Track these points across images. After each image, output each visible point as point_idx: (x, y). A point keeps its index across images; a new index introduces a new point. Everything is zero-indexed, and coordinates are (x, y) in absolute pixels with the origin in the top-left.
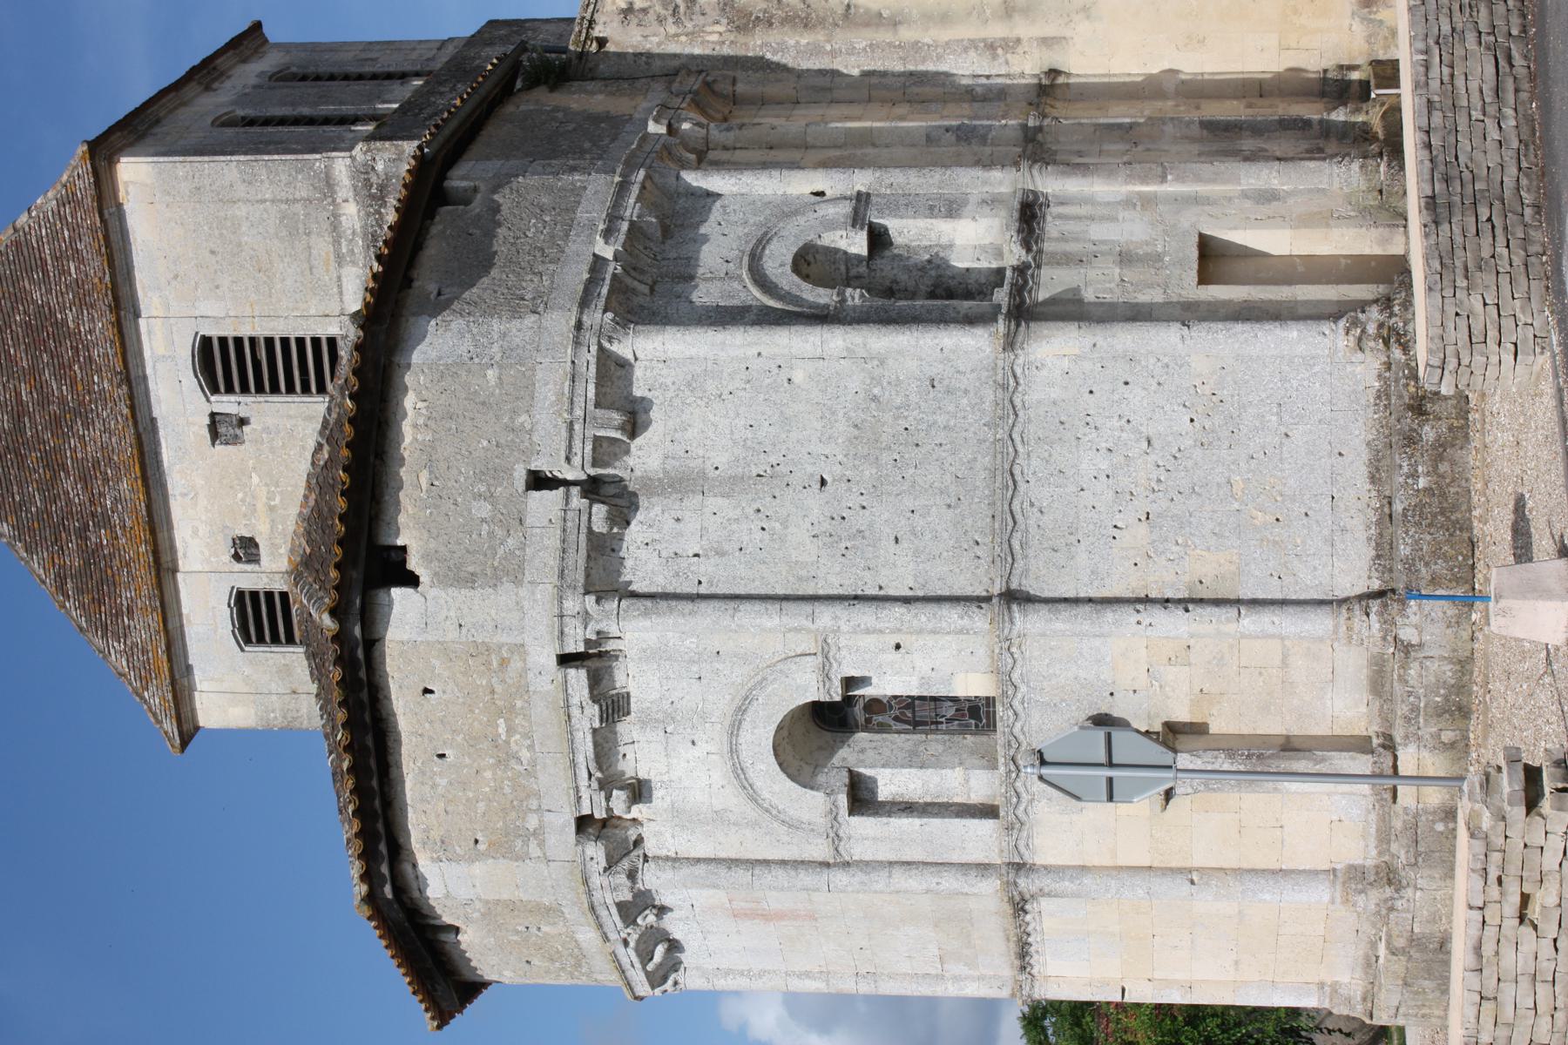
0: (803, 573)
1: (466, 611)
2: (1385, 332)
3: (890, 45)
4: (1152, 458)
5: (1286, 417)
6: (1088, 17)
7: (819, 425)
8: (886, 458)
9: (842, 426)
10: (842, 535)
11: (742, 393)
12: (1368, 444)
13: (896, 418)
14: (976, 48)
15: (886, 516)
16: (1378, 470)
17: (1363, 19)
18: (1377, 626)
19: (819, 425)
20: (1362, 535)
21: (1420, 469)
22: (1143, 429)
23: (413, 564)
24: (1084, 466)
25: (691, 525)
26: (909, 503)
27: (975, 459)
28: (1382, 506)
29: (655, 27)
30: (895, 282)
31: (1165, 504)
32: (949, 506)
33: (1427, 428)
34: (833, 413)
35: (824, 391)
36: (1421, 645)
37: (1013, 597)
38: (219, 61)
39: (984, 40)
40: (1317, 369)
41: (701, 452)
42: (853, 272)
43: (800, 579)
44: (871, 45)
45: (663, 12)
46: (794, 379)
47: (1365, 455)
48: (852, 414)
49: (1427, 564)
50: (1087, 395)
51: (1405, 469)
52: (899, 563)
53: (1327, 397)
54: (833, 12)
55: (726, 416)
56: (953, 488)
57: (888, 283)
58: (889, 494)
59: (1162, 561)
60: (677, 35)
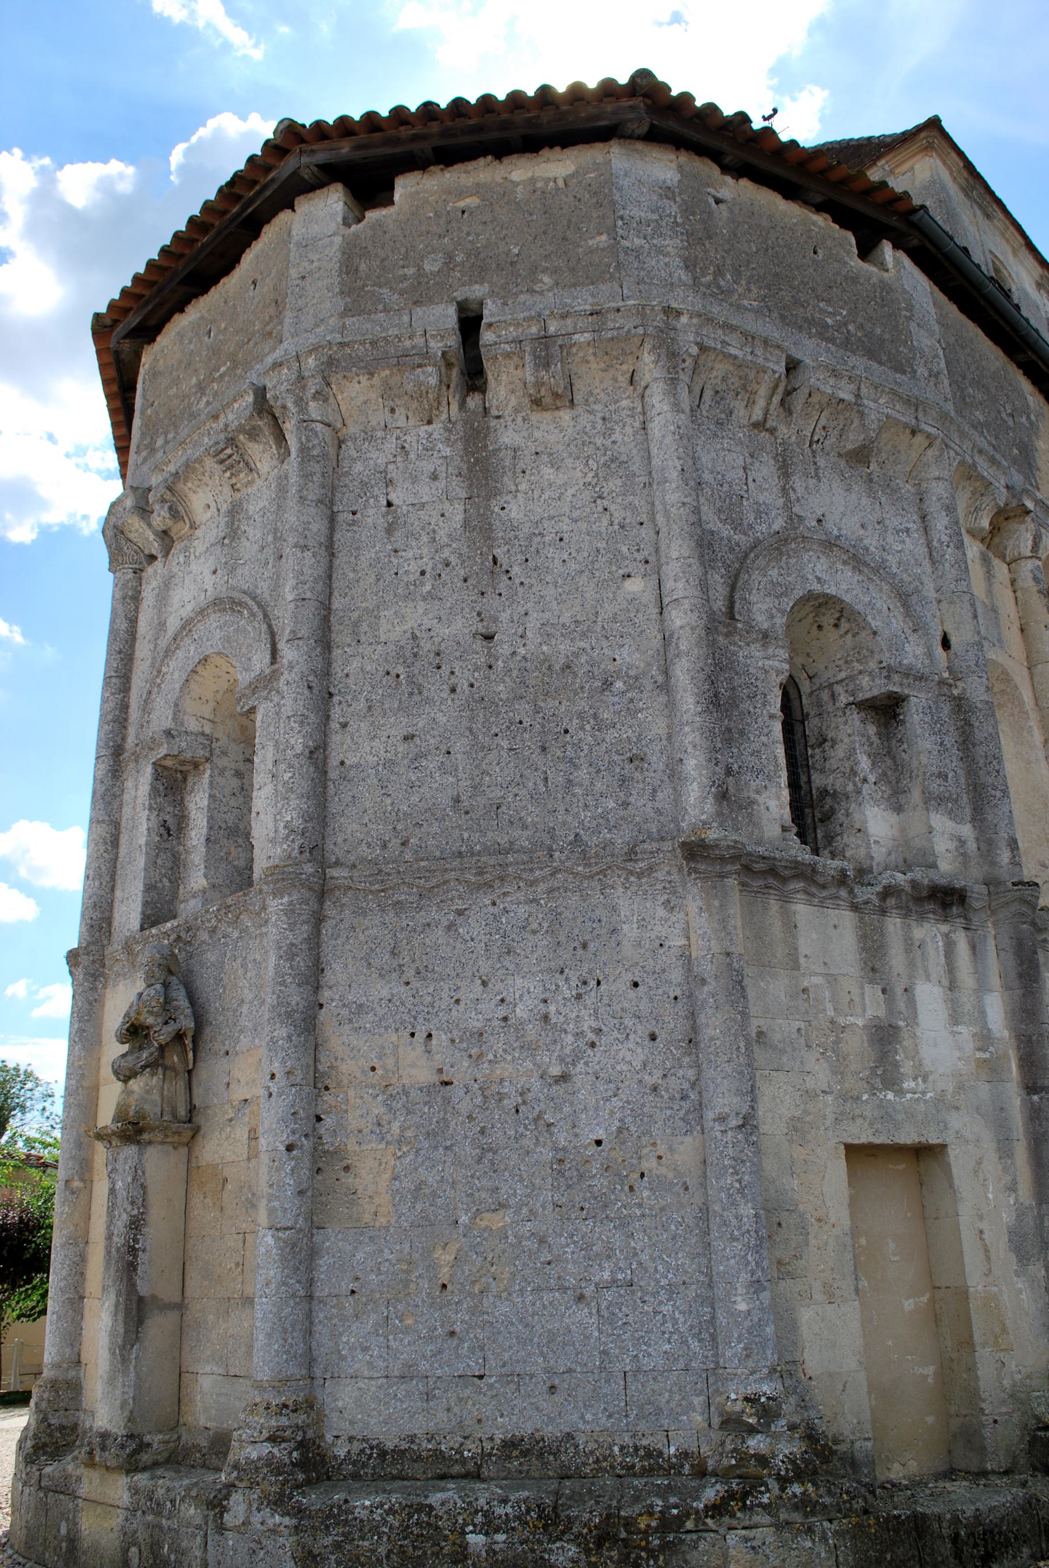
0: (364, 627)
1: (317, 275)
4: (536, 1084)
5: (608, 1296)
7: (566, 619)
8: (523, 710)
9: (565, 647)
10: (413, 669)
11: (605, 523)
12: (569, 1436)
13: (581, 716)
15: (442, 719)
16: (525, 1454)
18: (254, 1455)
19: (566, 619)
20: (419, 1426)
21: (501, 1537)
22: (580, 1066)
23: (372, 215)
24: (519, 982)
25: (426, 492)
26: (460, 746)
27: (525, 827)
28: (463, 1461)
30: (834, 743)
31: (464, 1107)
32: (457, 800)
33: (572, 1550)
34: (584, 635)
35: (614, 619)
36: (221, 1529)
37: (322, 892)
40: (694, 1345)
41: (523, 487)
42: (838, 689)
43: (356, 624)
47: (551, 1431)
48: (583, 659)
49: (337, 1546)
50: (629, 977)
51: (500, 1511)
52: (376, 743)
53: (647, 1363)
55: (574, 507)
56: (482, 801)
57: (831, 735)
58: (471, 719)
59: (378, 1109)
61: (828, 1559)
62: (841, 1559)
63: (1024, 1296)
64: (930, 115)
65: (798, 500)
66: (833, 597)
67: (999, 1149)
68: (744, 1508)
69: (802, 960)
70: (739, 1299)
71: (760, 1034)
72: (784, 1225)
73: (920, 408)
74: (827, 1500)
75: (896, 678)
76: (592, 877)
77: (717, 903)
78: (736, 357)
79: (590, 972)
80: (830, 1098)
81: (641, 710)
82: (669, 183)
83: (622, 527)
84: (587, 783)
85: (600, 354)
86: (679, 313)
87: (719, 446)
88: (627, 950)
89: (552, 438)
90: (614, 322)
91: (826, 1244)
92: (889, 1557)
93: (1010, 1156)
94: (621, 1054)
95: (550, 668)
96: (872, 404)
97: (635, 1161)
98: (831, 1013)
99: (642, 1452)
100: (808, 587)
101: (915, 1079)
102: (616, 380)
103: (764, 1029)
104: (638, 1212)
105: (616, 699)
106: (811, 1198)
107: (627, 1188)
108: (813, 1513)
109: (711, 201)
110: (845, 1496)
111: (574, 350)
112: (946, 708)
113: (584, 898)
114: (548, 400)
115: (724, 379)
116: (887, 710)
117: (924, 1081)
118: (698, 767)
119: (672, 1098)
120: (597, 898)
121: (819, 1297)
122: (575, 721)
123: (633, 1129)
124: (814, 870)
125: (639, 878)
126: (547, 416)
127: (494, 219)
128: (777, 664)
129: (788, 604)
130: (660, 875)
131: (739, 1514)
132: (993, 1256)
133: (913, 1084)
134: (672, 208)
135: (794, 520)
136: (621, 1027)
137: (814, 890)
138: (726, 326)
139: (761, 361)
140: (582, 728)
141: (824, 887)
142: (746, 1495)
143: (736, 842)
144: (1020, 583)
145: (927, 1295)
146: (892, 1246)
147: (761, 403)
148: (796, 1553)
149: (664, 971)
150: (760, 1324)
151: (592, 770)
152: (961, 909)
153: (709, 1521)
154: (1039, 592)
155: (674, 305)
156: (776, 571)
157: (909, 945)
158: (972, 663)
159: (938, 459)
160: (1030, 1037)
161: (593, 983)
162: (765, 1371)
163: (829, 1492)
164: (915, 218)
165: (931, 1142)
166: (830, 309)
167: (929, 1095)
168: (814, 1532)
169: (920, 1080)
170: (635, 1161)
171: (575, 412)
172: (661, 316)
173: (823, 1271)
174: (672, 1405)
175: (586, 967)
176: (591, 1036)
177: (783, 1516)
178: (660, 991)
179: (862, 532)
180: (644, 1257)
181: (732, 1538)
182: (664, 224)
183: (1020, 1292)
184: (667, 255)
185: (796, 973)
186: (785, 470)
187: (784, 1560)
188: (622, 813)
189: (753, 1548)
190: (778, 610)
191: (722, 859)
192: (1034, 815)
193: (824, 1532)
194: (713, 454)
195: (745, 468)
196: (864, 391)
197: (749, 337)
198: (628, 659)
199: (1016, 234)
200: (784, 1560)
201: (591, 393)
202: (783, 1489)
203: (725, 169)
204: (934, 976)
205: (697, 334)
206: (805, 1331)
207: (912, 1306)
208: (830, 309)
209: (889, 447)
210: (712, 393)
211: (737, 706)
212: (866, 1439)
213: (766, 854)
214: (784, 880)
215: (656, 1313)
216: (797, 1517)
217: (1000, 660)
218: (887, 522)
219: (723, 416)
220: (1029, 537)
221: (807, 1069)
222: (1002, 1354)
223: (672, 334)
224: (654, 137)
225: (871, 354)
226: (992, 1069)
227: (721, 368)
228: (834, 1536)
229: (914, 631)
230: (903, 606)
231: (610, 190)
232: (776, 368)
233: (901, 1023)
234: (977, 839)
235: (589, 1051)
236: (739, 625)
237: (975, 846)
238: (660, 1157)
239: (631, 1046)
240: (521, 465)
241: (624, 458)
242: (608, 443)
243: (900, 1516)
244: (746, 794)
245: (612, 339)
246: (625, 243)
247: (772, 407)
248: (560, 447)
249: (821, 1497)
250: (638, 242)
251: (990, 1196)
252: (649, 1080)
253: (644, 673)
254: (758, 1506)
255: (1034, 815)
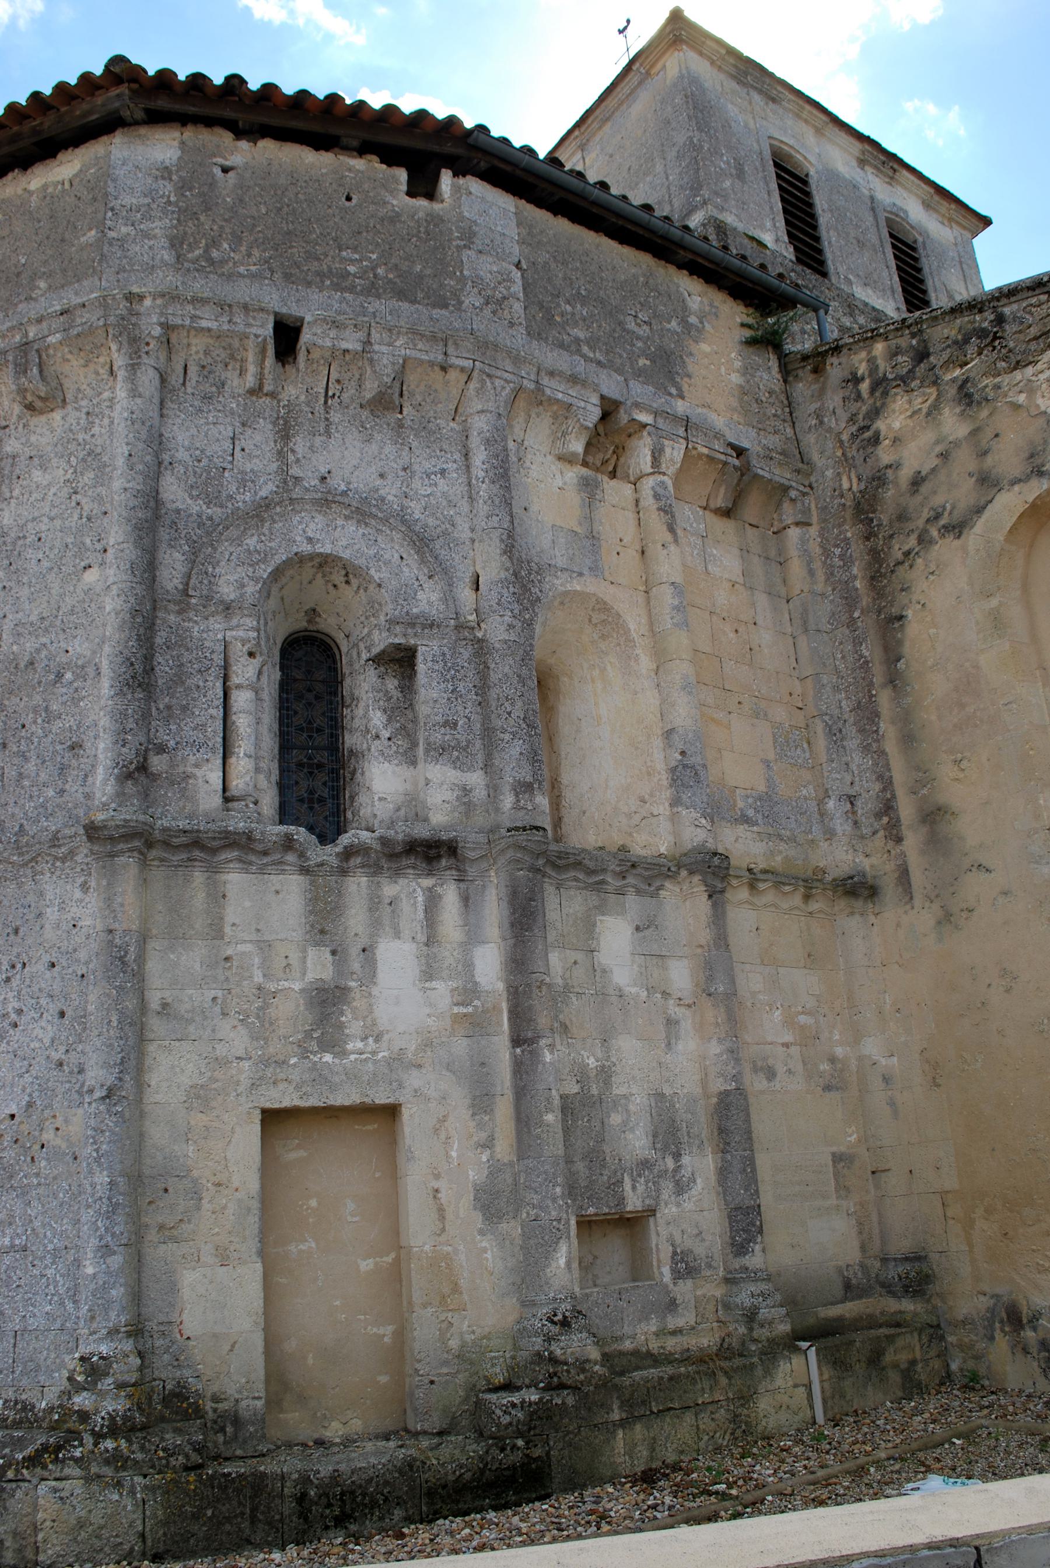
2: (72, 1424)
3: (871, 684)
6: (939, 923)
7: (34, 618)
9: (30, 645)
11: (76, 517)
13: (35, 710)
14: (884, 790)
17: (992, 1310)
19: (34, 618)
29: (844, 416)
33: (949, 1339)
35: (72, 612)
38: (905, 173)
39: (894, 796)
44: (867, 662)
45: (861, 417)
46: (89, 572)
48: (44, 653)
50: (46, 958)
54: (892, 603)
60: (841, 442)
61: (134, 1512)
62: (148, 1513)
63: (489, 1255)
64: (671, 8)
65: (298, 461)
66: (328, 556)
67: (473, 1106)
68: (56, 1460)
69: (228, 930)
70: (88, 1263)
71: (165, 1005)
72: (170, 1190)
73: (450, 343)
74: (139, 1456)
75: (398, 629)
76: (25, 865)
77: (104, 883)
78: (209, 330)
79: (18, 955)
80: (246, 1064)
81: (82, 699)
82: (167, 163)
83: (89, 519)
84: (33, 774)
85: (75, 351)
86: (141, 298)
87: (202, 421)
88: (49, 933)
89: (44, 441)
90: (83, 318)
91: (225, 1207)
92: (209, 1513)
93: (488, 1110)
94: (35, 1033)
95: (16, 667)
96: (384, 349)
97: (37, 1133)
98: (258, 978)
99: (19, 1407)
100: (295, 549)
101: (364, 1039)
102: (97, 373)
103: (169, 1000)
104: (35, 1182)
105: (64, 690)
106: (210, 1164)
107: (29, 1159)
108: (124, 1468)
109: (217, 171)
110: (161, 1453)
111: (51, 352)
112: (466, 653)
113: (20, 885)
114: (38, 404)
115: (206, 353)
116: (401, 661)
117: (377, 1040)
118: (106, 749)
119: (71, 1072)
120: (29, 885)
121: (207, 1258)
122: (31, 715)
123: (38, 1103)
124: (249, 838)
125: (63, 863)
126: (43, 418)
127: (11, 232)
128: (241, 633)
129: (265, 571)
130: (79, 858)
131: (50, 1466)
132: (449, 1215)
133: (360, 1045)
134: (167, 188)
135: (287, 481)
136: (37, 1007)
137: (253, 858)
138: (195, 300)
139: (241, 328)
140: (35, 722)
141: (265, 853)
142: (59, 1448)
143: (125, 820)
144: (642, 503)
145: (393, 1255)
146: (351, 1206)
147: (252, 369)
148: (103, 1505)
149: (75, 950)
150: (105, 1287)
151: (39, 761)
152: (452, 861)
153: (24, 1471)
154: (659, 509)
155: (135, 289)
156: (255, 538)
157: (374, 904)
158: (493, 603)
159: (480, 390)
160: (517, 988)
161: (19, 966)
162: (104, 1331)
163: (142, 1448)
164: (470, 141)
165: (377, 1102)
166: (357, 256)
167: (381, 1055)
168: (123, 1486)
169: (371, 1040)
170: (37, 1133)
171: (65, 411)
172: (124, 304)
173: (218, 1234)
174: (49, 1362)
175: (15, 950)
176: (13, 1016)
177: (94, 1469)
178: (70, 970)
179: (379, 482)
180: (37, 1224)
181: (43, 1488)
182: (154, 206)
183: (485, 1250)
184: (155, 237)
185: (217, 942)
186: (285, 433)
187: (90, 1511)
188: (58, 800)
189: (61, 1498)
190: (252, 578)
191: (111, 839)
192: (637, 748)
193: (133, 1486)
194: (194, 431)
195: (233, 439)
196: (375, 336)
197: (224, 306)
198: (79, 650)
199: (815, 112)
200: (90, 1511)
201: (79, 389)
202: (96, 1444)
203: (239, 133)
204: (406, 933)
205: (162, 314)
206: (186, 1293)
207: (371, 1266)
208: (357, 256)
209: (422, 387)
210: (197, 368)
211: (183, 683)
212: (254, 1398)
213: (188, 827)
214: (214, 851)
215: (43, 1276)
216: (108, 1471)
217: (591, 589)
218: (416, 467)
219: (214, 389)
220: (647, 452)
221: (219, 1036)
222: (450, 1314)
223: (134, 320)
224: (156, 118)
225: (401, 295)
226: (475, 1025)
227: (198, 344)
228: (142, 1491)
229: (430, 577)
230: (417, 553)
231: (106, 182)
232: (260, 331)
233: (353, 984)
234: (488, 786)
235: (11, 1032)
236: (193, 601)
237: (484, 793)
238: (57, 1129)
239: (43, 1024)
240: (17, 472)
241: (99, 450)
242: (88, 437)
243: (230, 1474)
244: (181, 769)
245: (78, 335)
246: (112, 234)
247: (266, 371)
248: (49, 448)
249: (133, 1452)
250: (124, 230)
251: (454, 1154)
252: (56, 1056)
253: (89, 662)
254: (70, 1459)
255: (637, 748)
